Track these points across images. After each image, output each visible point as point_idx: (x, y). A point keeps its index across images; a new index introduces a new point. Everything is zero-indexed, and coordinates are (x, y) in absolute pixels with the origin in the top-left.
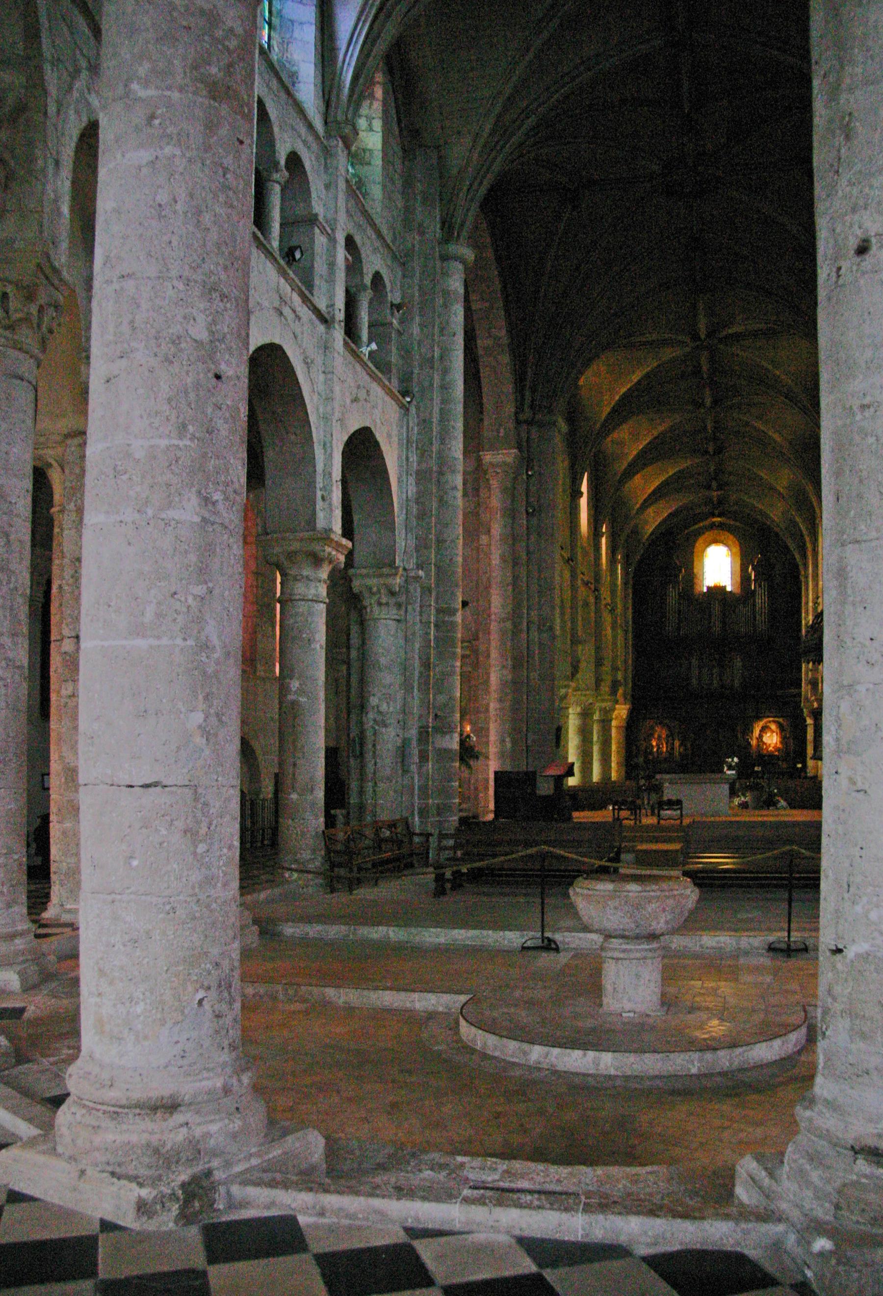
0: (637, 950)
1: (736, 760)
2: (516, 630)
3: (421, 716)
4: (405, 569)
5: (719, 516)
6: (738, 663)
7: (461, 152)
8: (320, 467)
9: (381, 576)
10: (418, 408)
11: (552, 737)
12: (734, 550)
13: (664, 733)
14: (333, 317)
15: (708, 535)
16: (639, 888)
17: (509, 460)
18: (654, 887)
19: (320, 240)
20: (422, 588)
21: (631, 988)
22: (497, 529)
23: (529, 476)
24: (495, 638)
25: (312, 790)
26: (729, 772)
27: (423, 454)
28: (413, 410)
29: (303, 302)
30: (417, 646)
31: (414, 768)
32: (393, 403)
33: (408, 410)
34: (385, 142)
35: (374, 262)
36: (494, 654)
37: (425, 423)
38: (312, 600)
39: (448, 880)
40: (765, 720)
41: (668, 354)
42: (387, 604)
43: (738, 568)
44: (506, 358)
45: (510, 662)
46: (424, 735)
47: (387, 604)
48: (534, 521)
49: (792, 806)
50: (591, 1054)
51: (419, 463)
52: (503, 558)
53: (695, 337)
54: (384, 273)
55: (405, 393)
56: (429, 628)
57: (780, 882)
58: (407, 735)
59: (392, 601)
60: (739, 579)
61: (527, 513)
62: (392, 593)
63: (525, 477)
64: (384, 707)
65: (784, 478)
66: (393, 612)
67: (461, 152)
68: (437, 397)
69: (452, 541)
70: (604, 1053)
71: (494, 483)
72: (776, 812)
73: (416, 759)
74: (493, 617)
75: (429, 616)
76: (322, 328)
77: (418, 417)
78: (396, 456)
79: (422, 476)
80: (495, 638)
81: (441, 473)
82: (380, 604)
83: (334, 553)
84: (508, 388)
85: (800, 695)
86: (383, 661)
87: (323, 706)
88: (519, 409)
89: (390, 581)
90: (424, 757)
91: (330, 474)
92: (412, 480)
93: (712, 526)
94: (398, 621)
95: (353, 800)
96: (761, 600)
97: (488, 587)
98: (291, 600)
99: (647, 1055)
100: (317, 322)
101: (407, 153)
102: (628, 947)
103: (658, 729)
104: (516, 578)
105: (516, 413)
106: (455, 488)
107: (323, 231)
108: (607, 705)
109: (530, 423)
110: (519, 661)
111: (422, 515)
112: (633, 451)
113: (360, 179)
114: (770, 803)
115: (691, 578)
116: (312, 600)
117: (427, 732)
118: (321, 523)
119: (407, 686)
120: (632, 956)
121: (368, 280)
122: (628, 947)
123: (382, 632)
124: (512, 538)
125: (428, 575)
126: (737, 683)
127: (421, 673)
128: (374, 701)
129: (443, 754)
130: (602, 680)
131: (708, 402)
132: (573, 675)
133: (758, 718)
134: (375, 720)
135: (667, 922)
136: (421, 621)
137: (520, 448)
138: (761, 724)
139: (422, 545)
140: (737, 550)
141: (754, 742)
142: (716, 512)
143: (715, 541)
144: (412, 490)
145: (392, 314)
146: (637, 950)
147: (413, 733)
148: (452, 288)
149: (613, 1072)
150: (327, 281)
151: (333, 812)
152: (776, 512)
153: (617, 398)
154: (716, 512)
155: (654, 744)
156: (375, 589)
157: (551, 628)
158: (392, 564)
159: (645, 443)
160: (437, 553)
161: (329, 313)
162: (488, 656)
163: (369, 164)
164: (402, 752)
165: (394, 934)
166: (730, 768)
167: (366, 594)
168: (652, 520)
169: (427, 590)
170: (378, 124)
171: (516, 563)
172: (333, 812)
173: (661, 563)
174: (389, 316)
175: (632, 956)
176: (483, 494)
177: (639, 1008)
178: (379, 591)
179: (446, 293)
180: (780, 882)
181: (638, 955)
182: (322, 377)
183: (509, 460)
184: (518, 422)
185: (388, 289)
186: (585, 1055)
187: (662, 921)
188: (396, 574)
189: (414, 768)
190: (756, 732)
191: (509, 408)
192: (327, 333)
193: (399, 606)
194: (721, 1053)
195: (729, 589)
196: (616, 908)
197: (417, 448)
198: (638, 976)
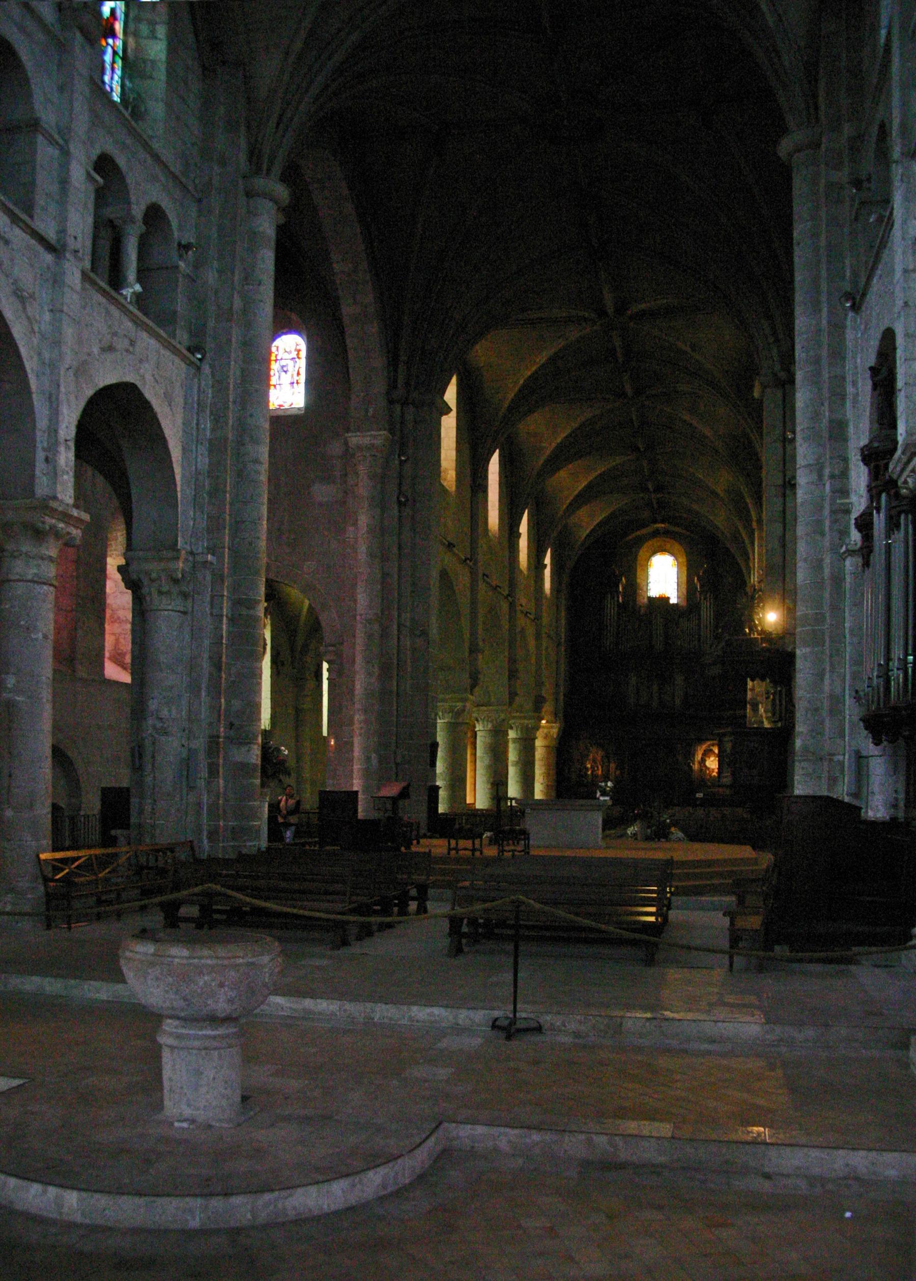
0: (197, 1037)
1: (609, 784)
2: (384, 634)
3: (210, 724)
4: (192, 553)
5: (663, 522)
6: (679, 680)
7: (269, 69)
8: (42, 423)
9: (161, 559)
10: (212, 367)
11: (427, 755)
12: (680, 560)
13: (601, 753)
14: (64, 246)
15: (655, 542)
16: (186, 953)
17: (378, 442)
18: (206, 952)
19: (45, 153)
20: (213, 574)
21: (196, 1087)
22: (363, 520)
23: (401, 462)
24: (360, 640)
25: (31, 807)
26: (602, 798)
27: (218, 419)
28: (206, 369)
29: (13, 222)
30: (207, 642)
31: (201, 783)
32: (177, 360)
33: (199, 369)
34: (172, 51)
35: (145, 190)
36: (359, 660)
37: (220, 386)
38: (32, 581)
39: (413, 899)
40: (709, 743)
41: (574, 334)
42: (168, 593)
43: (684, 578)
44: (374, 328)
45: (376, 670)
46: (213, 744)
47: (168, 593)
48: (408, 511)
49: (694, 837)
50: (52, 1191)
51: (213, 430)
52: (371, 555)
53: (602, 313)
54: (166, 204)
55: (192, 350)
56: (221, 621)
57: (554, 934)
58: (193, 746)
59: (175, 590)
60: (685, 591)
61: (399, 502)
62: (176, 581)
63: (397, 462)
64: (165, 713)
65: (722, 480)
66: (178, 604)
67: (269, 69)
68: (235, 353)
69: (253, 522)
70: (68, 1191)
71: (362, 469)
72: (668, 845)
73: (204, 774)
74: (358, 618)
75: (222, 608)
76: (49, 258)
77: (213, 376)
78: (179, 421)
79: (216, 447)
80: (360, 640)
81: (240, 443)
82: (160, 593)
83: (61, 525)
84: (379, 362)
85: (745, 716)
86: (163, 658)
87: (48, 707)
88: (393, 385)
89: (172, 565)
90: (213, 771)
91: (56, 431)
92: (203, 450)
93: (656, 534)
94: (185, 613)
95: (133, 820)
96: (707, 612)
97: (354, 586)
98: (9, 581)
99: (125, 1197)
100: (40, 249)
101: (207, 71)
102: (183, 1031)
103: (593, 749)
104: (385, 575)
105: (388, 393)
106: (257, 461)
107: (52, 141)
108: (530, 723)
109: (405, 403)
110: (387, 668)
111: (216, 492)
112: (549, 446)
113: (139, 95)
114: (661, 834)
115: (634, 587)
116: (32, 581)
117: (218, 743)
118: (42, 488)
119: (194, 688)
120: (190, 1043)
121: (138, 211)
122: (183, 1031)
123: (163, 626)
124: (379, 531)
125: (220, 559)
126: (678, 702)
127: (210, 674)
128: (153, 705)
129: (244, 768)
130: (516, 694)
131: (629, 390)
132: (473, 686)
133: (701, 741)
134: (154, 727)
135: (231, 1001)
136: (211, 614)
137: (392, 431)
138: (704, 747)
139: (215, 526)
140: (683, 560)
141: (696, 767)
142: (659, 518)
143: (662, 550)
144: (203, 462)
145: (181, 256)
146: (197, 1037)
147: (200, 744)
148: (261, 229)
149: (79, 1219)
150: (57, 202)
151: (113, 832)
152: (720, 519)
153: (522, 382)
154: (659, 518)
155: (589, 766)
156: (154, 575)
157: (424, 633)
158: (174, 547)
159: (564, 435)
160: (233, 536)
161: (58, 240)
162: (354, 661)
163: (151, 77)
164: (187, 764)
165: (51, 986)
166: (604, 793)
167: (146, 582)
168: (587, 521)
169: (219, 578)
170: (161, 31)
171: (384, 558)
172: (113, 832)
173: (599, 571)
174: (176, 258)
175: (190, 1043)
176: (351, 480)
177: (202, 1116)
178: (159, 578)
179: (253, 235)
180: (554, 934)
181: (197, 1043)
182: (47, 316)
183: (378, 442)
184: (391, 402)
185: (174, 224)
186: (45, 1192)
187: (222, 998)
188: (178, 558)
189: (201, 783)
190: (699, 757)
191: (379, 386)
192: (57, 264)
193: (185, 596)
194: (236, 1200)
195: (674, 600)
196: (157, 979)
197: (211, 413)
198: (198, 1073)
